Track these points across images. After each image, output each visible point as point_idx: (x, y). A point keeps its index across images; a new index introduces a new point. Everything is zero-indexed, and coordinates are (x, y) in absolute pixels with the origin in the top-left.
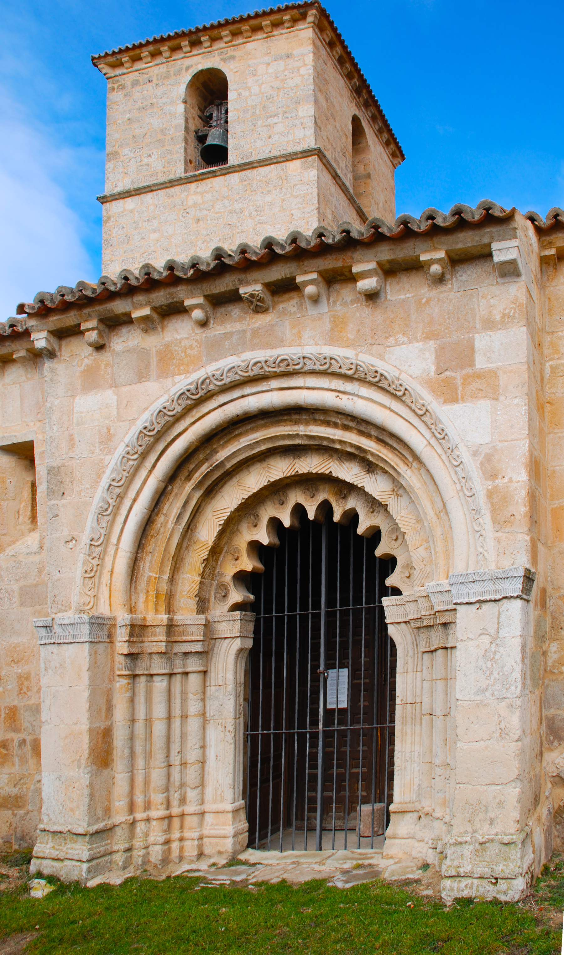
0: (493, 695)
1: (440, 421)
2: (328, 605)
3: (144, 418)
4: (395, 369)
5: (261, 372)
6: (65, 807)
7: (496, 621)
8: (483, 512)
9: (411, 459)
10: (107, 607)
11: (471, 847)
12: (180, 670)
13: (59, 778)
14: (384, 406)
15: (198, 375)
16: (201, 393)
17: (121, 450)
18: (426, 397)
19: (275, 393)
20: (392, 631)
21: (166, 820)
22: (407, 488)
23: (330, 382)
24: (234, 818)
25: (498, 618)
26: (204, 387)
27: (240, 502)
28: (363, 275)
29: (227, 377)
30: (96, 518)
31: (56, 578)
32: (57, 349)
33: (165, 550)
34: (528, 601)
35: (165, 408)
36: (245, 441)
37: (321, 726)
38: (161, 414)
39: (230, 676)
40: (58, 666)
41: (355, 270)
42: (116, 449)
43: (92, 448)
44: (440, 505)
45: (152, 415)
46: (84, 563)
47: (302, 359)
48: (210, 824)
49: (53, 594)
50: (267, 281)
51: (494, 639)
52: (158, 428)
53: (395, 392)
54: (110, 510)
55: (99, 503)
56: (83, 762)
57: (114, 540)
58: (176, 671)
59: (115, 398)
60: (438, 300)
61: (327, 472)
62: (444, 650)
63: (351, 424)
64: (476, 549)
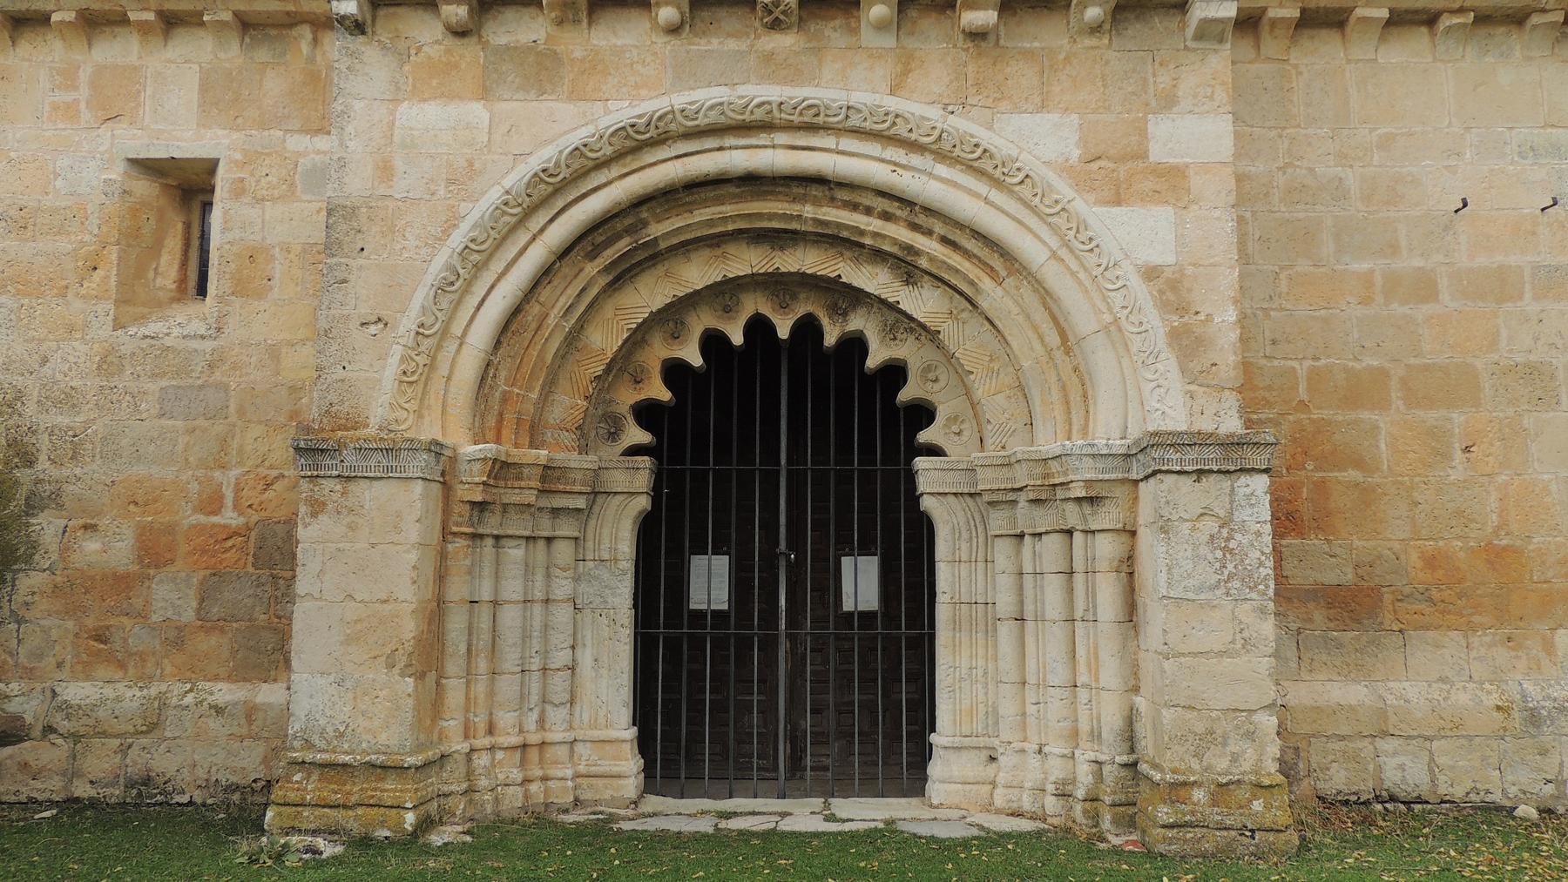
12: (546, 534)
16: (652, 133)
17: (494, 196)
18: (1064, 189)
20: (927, 503)
30: (432, 293)
32: (369, 22)
42: (484, 193)
44: (1053, 339)
45: (561, 152)
46: (403, 359)
54: (458, 285)
57: (457, 329)
58: (537, 533)
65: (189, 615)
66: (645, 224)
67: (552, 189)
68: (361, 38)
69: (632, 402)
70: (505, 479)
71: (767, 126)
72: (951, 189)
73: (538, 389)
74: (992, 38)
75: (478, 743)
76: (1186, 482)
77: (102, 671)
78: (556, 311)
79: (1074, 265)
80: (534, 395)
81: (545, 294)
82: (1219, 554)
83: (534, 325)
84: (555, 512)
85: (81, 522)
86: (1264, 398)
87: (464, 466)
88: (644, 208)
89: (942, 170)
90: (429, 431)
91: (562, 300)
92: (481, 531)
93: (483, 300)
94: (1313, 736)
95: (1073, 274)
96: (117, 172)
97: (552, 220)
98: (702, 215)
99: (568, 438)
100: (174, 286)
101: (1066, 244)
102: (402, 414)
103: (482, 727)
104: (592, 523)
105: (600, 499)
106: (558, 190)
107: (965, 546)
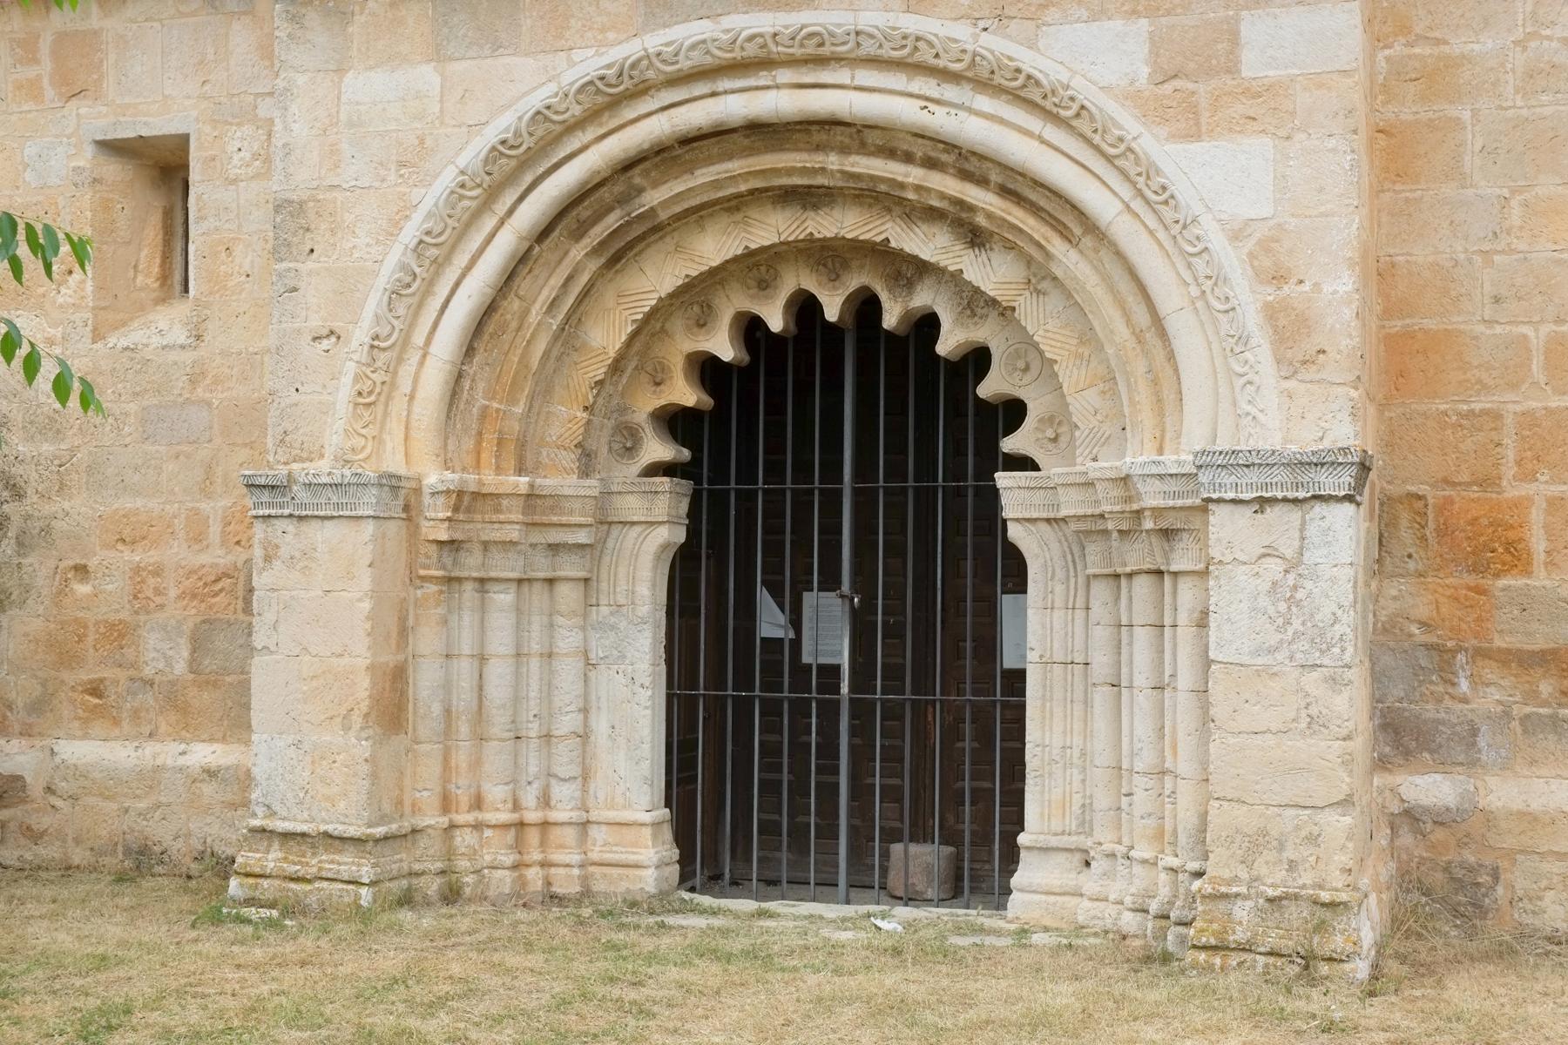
1: (1158, 172)
2: (858, 475)
3: (501, 125)
4: (1060, 67)
5: (762, 54)
6: (311, 793)
7: (1297, 535)
8: (1253, 342)
9: (1077, 231)
10: (400, 457)
11: (1249, 904)
12: (541, 575)
13: (297, 745)
15: (630, 50)
17: (447, 179)
18: (1129, 123)
20: (1015, 533)
21: (513, 831)
22: (1067, 282)
24: (655, 836)
26: (634, 73)
27: (680, 282)
29: (687, 58)
30: (386, 298)
31: (288, 401)
33: (520, 362)
34: (1358, 504)
35: (548, 108)
36: (705, 175)
37: (845, 689)
38: (540, 117)
39: (644, 590)
40: (297, 554)
42: (436, 176)
44: (1142, 317)
45: (520, 118)
46: (357, 378)
47: (853, 35)
48: (600, 842)
49: (280, 429)
52: (528, 142)
53: (1055, 110)
54: (415, 286)
55: (393, 272)
56: (356, 719)
57: (419, 338)
59: (437, 80)
61: (878, 239)
63: (944, 157)
64: (1235, 404)
65: (180, 668)
66: (640, 191)
67: (518, 162)
69: (650, 409)
70: (482, 513)
73: (522, 404)
75: (461, 818)
76: (1247, 511)
77: (98, 728)
78: (537, 306)
79: (1151, 222)
80: (519, 409)
81: (524, 285)
82: (1283, 606)
83: (514, 324)
84: (554, 548)
85: (71, 563)
86: (1479, 381)
87: (427, 500)
88: (637, 170)
89: (984, 102)
90: (394, 463)
91: (545, 293)
96: (86, 156)
97: (521, 199)
98: (705, 177)
99: (569, 459)
100: (156, 285)
101: (1140, 193)
104: (606, 559)
105: (615, 530)
106: (525, 163)
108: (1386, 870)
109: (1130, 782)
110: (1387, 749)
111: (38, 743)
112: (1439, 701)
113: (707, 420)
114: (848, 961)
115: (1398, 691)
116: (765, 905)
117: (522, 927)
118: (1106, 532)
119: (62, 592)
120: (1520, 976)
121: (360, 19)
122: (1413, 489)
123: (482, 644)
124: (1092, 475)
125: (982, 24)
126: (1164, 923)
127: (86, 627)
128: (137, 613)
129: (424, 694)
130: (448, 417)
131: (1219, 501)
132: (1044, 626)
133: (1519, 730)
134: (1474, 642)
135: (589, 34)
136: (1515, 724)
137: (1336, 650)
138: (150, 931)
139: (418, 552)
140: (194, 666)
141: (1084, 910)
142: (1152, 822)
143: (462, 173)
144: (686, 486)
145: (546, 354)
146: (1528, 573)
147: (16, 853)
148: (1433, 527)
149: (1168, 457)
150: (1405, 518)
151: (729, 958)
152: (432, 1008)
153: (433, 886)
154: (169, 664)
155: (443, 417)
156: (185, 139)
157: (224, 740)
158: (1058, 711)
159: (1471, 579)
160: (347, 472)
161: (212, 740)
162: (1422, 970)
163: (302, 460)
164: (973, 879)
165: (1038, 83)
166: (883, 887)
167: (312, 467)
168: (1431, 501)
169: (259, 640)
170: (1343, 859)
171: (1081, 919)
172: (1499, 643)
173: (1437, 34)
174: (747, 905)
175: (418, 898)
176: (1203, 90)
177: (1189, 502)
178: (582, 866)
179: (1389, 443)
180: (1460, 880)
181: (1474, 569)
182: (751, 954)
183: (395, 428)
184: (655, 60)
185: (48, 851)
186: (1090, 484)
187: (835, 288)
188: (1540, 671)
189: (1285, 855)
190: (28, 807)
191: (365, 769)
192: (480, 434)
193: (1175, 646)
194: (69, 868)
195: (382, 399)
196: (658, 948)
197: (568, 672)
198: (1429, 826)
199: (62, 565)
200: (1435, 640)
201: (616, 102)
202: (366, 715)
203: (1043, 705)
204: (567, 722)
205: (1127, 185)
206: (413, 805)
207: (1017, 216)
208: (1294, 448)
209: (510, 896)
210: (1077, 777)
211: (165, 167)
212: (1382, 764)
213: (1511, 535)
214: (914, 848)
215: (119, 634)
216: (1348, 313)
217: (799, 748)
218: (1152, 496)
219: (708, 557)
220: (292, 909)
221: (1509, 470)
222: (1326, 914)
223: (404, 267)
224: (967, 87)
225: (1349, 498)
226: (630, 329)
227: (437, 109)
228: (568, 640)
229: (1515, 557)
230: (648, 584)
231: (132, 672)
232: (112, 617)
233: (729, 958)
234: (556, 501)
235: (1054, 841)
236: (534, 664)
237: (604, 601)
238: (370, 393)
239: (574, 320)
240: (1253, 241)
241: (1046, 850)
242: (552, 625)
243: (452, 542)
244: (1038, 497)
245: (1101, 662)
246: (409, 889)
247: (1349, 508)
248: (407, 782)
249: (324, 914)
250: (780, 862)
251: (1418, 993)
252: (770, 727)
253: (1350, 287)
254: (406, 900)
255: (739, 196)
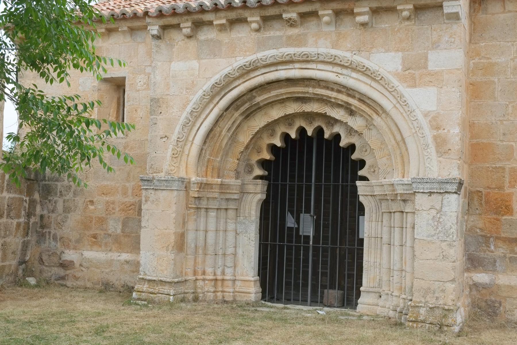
0: (438, 238)
3: (216, 78)
5: (291, 59)
7: (440, 203)
8: (430, 146)
9: (381, 112)
10: (184, 172)
11: (425, 309)
12: (224, 207)
13: (153, 255)
14: (367, 84)
16: (252, 67)
17: (200, 93)
18: (395, 82)
19: (297, 70)
20: (362, 199)
23: (333, 68)
24: (255, 284)
25: (442, 201)
27: (266, 123)
28: (360, 14)
30: (181, 127)
32: (162, 35)
34: (459, 194)
36: (274, 93)
37: (311, 243)
39: (253, 212)
40: (155, 200)
41: (355, 11)
43: (182, 91)
44: (399, 138)
45: (221, 76)
46: (173, 150)
47: (317, 55)
49: (150, 164)
50: (300, 12)
51: (439, 211)
56: (170, 248)
57: (191, 139)
59: (198, 65)
60: (406, 30)
61: (323, 112)
62: (400, 213)
63: (343, 90)
65: (119, 231)
66: (255, 97)
68: (160, 41)
69: (256, 160)
71: (292, 62)
72: (358, 82)
74: (370, 25)
76: (426, 196)
78: (225, 130)
79: (402, 111)
80: (218, 159)
81: (221, 123)
82: (436, 223)
83: (218, 135)
84: (227, 200)
85: (89, 200)
86: (498, 158)
87: (192, 185)
88: (254, 91)
89: (354, 75)
90: (183, 174)
91: (227, 126)
92: (199, 206)
93: (199, 128)
94: (508, 297)
95: (402, 114)
97: (221, 99)
99: (232, 174)
101: (398, 102)
102: (173, 168)
103: (200, 272)
104: (243, 203)
106: (222, 89)
107: (374, 216)
108: (468, 301)
109: (393, 273)
110: (469, 266)
111: (78, 252)
112: (485, 252)
113: (273, 163)
114: (309, 322)
115: (473, 249)
116: (286, 306)
117: (216, 309)
118: (387, 199)
119: (86, 208)
120: (505, 333)
121: (176, 47)
122: (478, 189)
123: (206, 227)
124: (383, 183)
125: (354, 53)
126: (401, 314)
127: (92, 218)
128: (107, 215)
129: (189, 241)
130: (198, 161)
131: (418, 192)
132: (369, 227)
133: (508, 261)
134: (496, 235)
135: (241, 53)
136: (507, 259)
137: (451, 236)
138: (111, 306)
139: (189, 200)
140: (123, 231)
141: (379, 310)
142: (399, 285)
143: (204, 91)
144: (266, 182)
145: (227, 143)
146: (512, 215)
147: (71, 283)
148: (483, 201)
149: (405, 179)
150: (476, 198)
151: (275, 320)
152: (191, 330)
153: (191, 297)
154: (116, 230)
155: (197, 161)
156: (125, 78)
157: (131, 252)
158: (373, 251)
159: (495, 216)
160: (170, 177)
161: (127, 252)
162: (476, 330)
163: (157, 173)
164: (347, 301)
165: (369, 70)
166: (321, 302)
167: (159, 175)
168: (483, 193)
169: (143, 224)
170: (452, 297)
171: (378, 313)
172: (503, 235)
173: (488, 56)
174: (281, 305)
175: (186, 300)
176: (417, 73)
177: (411, 192)
178: (233, 292)
179: (472, 175)
180: (490, 305)
181: (496, 213)
182: (281, 319)
183: (183, 164)
184: (260, 60)
185: (80, 283)
186: (383, 185)
187: (311, 126)
188: (515, 244)
189: (435, 295)
190: (75, 270)
191: (172, 262)
192: (207, 166)
193: (406, 233)
194: (86, 288)
195: (180, 156)
196: (254, 316)
197: (231, 236)
198: (481, 289)
199: (86, 200)
200: (484, 234)
201: (249, 72)
202: (173, 247)
203: (369, 250)
204: (230, 250)
205: (395, 100)
206: (186, 273)
207: (363, 107)
208: (440, 178)
209: (212, 300)
210: (378, 271)
211: (118, 86)
212: (468, 270)
213: (507, 204)
214: (331, 291)
215: (102, 221)
216: (457, 139)
217: (297, 260)
218: (400, 190)
219: (272, 203)
220: (151, 301)
221: (507, 184)
222: (447, 313)
223: (187, 118)
224: (349, 70)
225: (456, 193)
226: (251, 137)
227: (197, 73)
228: (231, 226)
229: (509, 210)
230: (254, 211)
231: (105, 232)
232: (100, 216)
233: (275, 320)
234: (228, 186)
235: (371, 290)
236: (221, 233)
237: (241, 215)
238: (176, 154)
239: (235, 134)
240: (431, 117)
241: (368, 292)
242: (226, 222)
243: (199, 197)
244: (368, 189)
245: (385, 237)
246: (184, 297)
247: (456, 196)
248: (184, 266)
249: (160, 304)
250: (291, 293)
251: (472, 336)
252: (289, 254)
253: (458, 131)
254: (183, 300)
255: (284, 99)
